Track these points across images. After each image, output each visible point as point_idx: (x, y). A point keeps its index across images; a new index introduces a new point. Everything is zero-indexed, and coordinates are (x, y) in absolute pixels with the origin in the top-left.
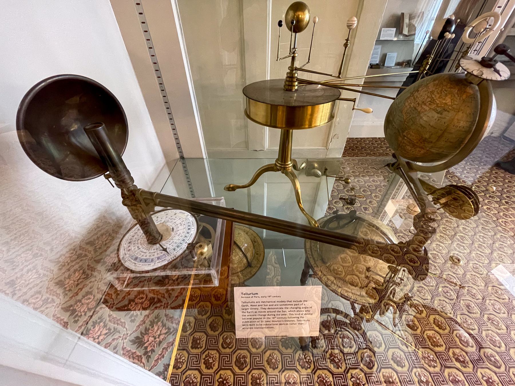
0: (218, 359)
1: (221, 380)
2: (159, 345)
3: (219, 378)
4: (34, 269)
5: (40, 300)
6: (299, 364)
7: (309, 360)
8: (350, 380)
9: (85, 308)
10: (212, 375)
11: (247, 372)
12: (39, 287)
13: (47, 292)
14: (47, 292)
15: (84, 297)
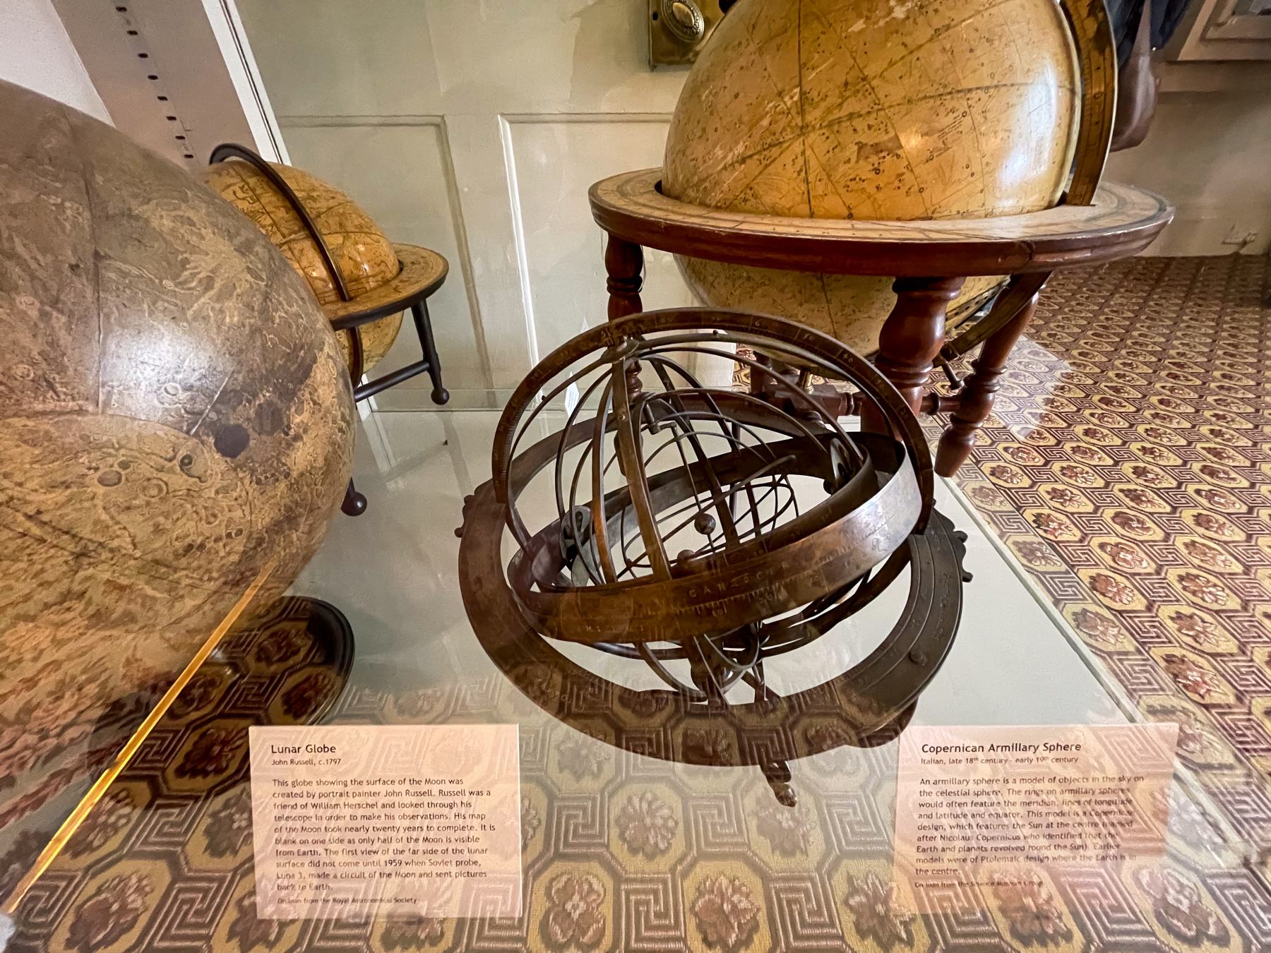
2: (45, 762)
5: (80, 615)
6: (622, 836)
7: (665, 820)
8: (846, 902)
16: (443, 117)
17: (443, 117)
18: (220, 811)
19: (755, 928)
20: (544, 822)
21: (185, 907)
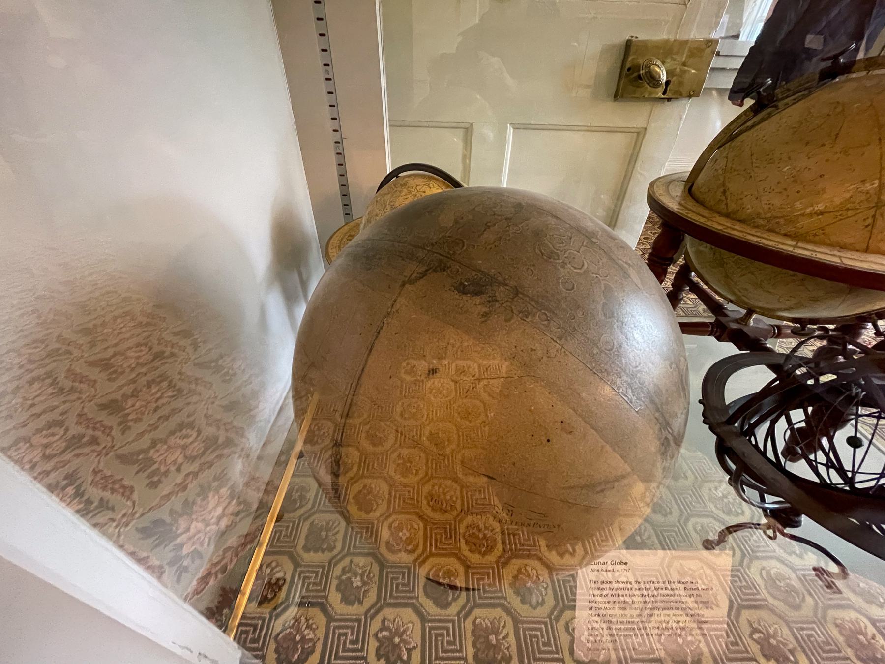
0: (376, 579)
1: (386, 633)
3: (381, 630)
4: (49, 377)
9: (177, 455)
10: (359, 621)
11: (458, 614)
12: (58, 411)
13: (79, 423)
14: (79, 423)
15: (172, 433)
16: (472, 124)
17: (472, 124)
18: (341, 576)
19: (312, 651)
20: (550, 584)
21: (244, 636)
